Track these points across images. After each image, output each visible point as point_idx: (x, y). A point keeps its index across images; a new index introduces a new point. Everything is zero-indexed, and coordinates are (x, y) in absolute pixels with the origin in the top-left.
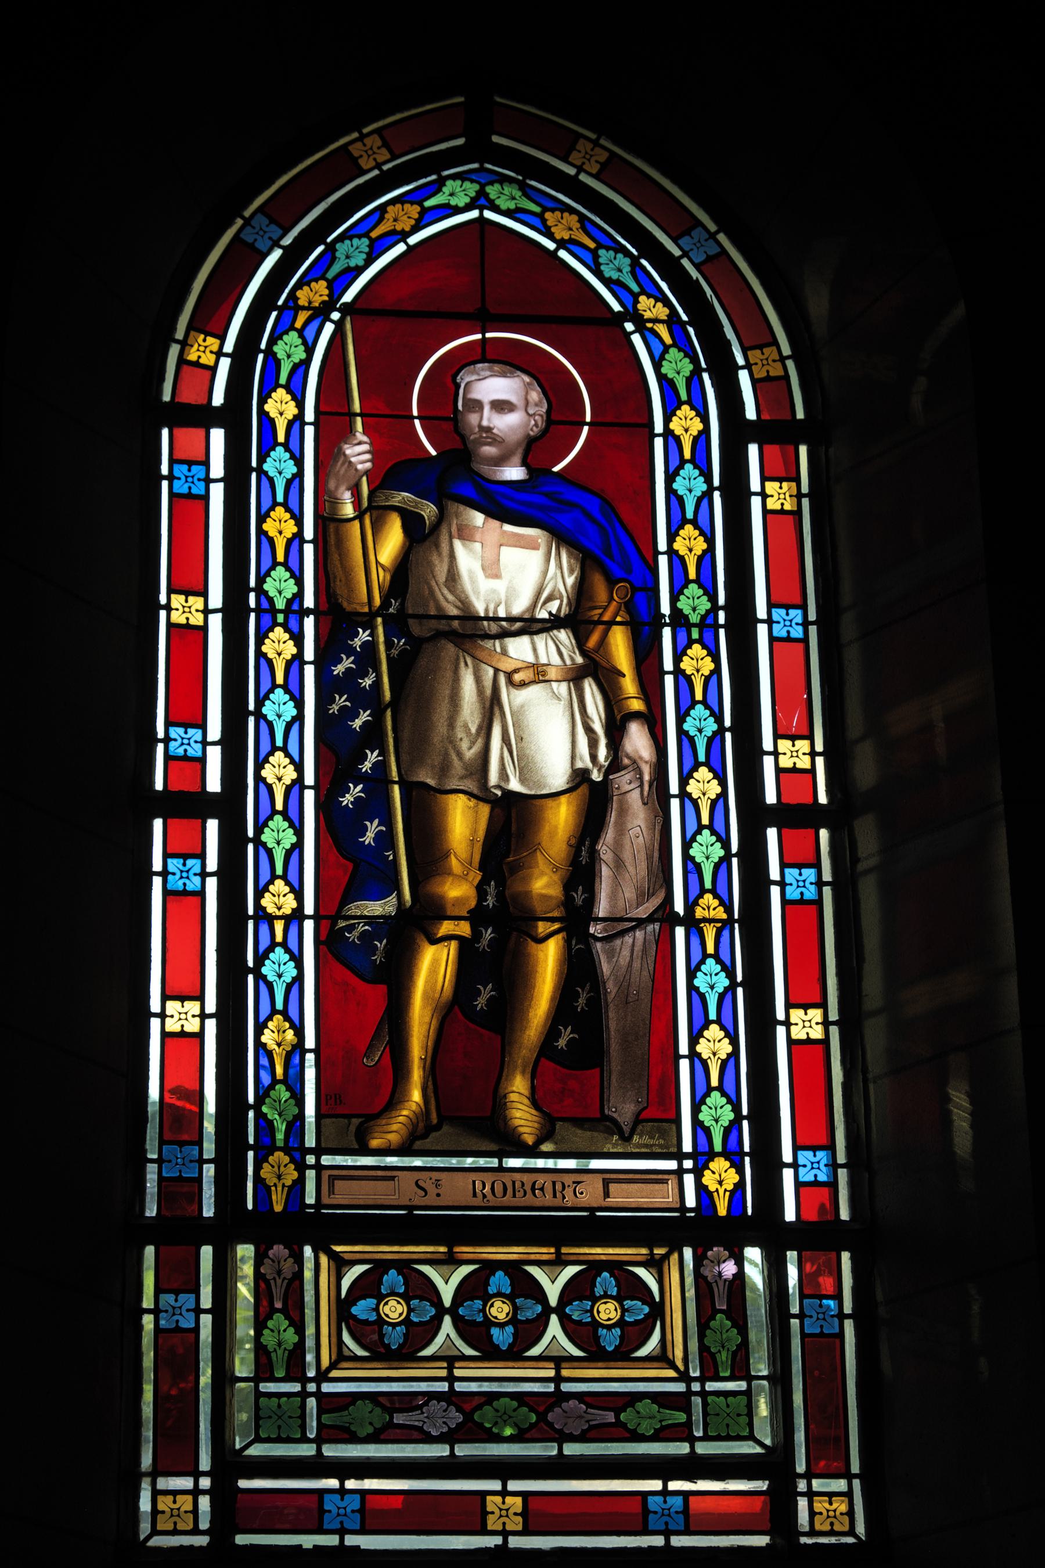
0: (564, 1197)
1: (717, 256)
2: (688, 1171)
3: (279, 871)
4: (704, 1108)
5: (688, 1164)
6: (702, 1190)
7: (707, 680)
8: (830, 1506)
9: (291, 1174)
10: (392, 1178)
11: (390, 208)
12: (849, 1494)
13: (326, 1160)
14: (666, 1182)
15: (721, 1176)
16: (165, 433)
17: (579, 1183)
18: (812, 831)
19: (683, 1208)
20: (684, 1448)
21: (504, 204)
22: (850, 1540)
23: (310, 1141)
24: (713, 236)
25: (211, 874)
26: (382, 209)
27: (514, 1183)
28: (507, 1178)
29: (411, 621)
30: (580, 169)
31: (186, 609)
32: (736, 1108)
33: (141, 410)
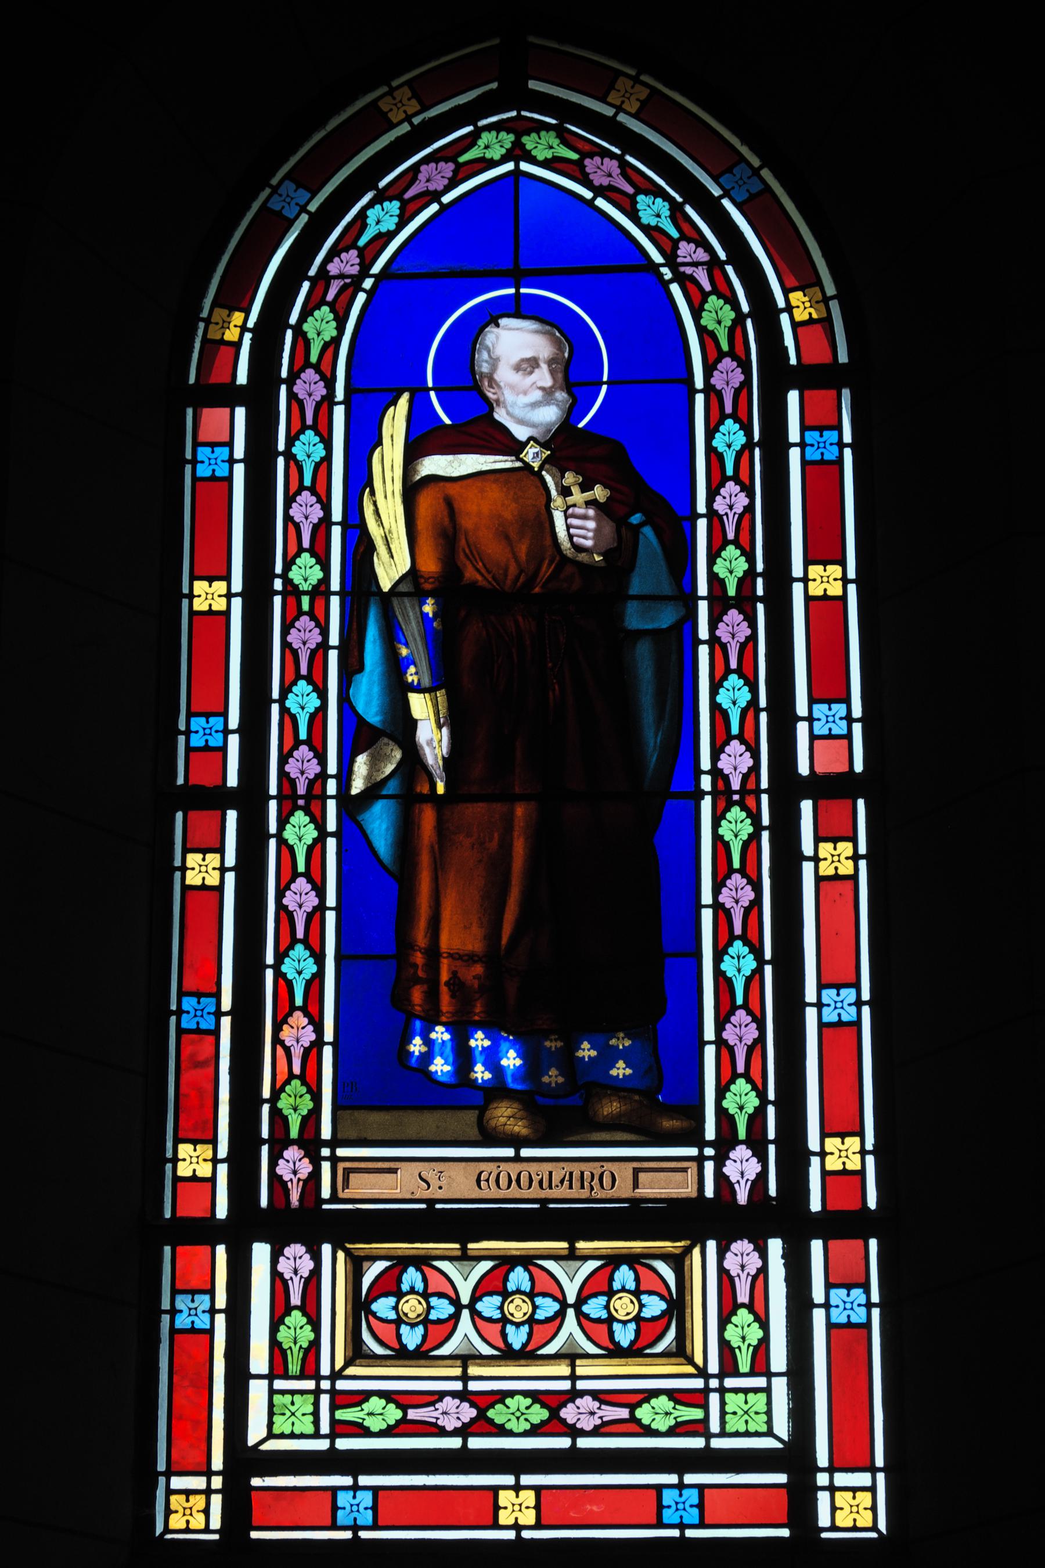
1: (760, 193)
2: (709, 1158)
5: (709, 1152)
6: (721, 1178)
7: (750, 1050)
8: (853, 1506)
9: (305, 1168)
11: (423, 168)
12: (872, 1489)
13: (341, 1152)
14: (684, 1170)
15: (742, 1166)
16: (179, 816)
18: (850, 801)
20: (698, 1443)
21: (541, 154)
22: (874, 1535)
23: (326, 1133)
24: (756, 172)
25: (236, 595)
26: (415, 168)
30: (619, 109)
31: (193, 1311)
32: (762, 1094)
33: (172, 392)
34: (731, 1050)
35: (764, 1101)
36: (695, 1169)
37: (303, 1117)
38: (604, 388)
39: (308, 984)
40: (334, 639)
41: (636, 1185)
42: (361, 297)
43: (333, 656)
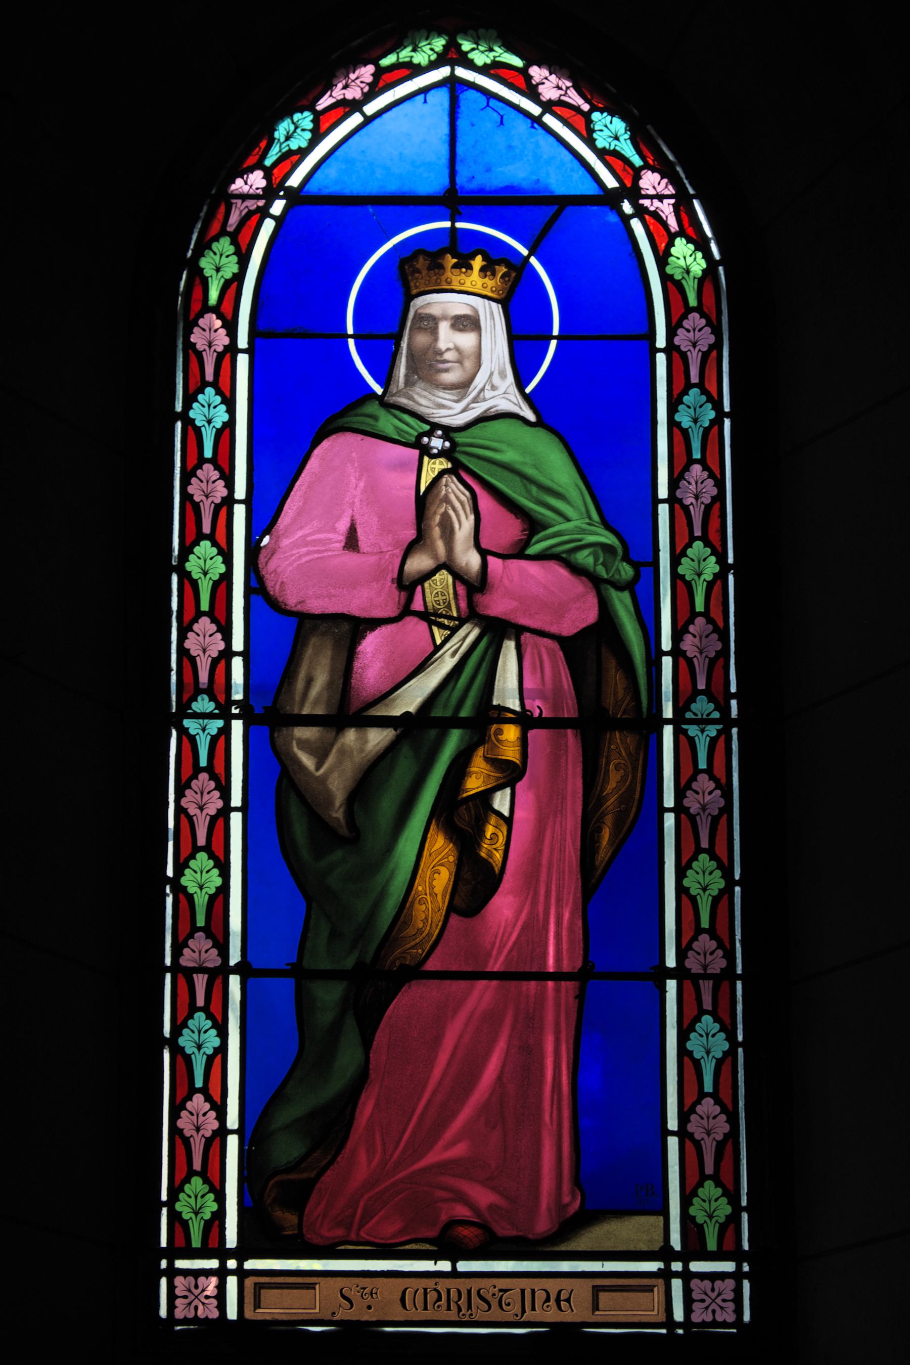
0: (460, 1310)
3: (709, 1169)
4: (695, 1200)
7: (705, 356)
10: (311, 1286)
14: (650, 1289)
17: (505, 1291)
19: (670, 1323)
27: (449, 1291)
28: (463, 1284)
29: (508, 791)
34: (684, 356)
35: (730, 883)
36: (662, 1289)
37: (217, 430)
38: (553, 344)
39: (219, 433)
40: (240, 492)
41: (596, 1307)
42: (269, 226)
43: (240, 511)
